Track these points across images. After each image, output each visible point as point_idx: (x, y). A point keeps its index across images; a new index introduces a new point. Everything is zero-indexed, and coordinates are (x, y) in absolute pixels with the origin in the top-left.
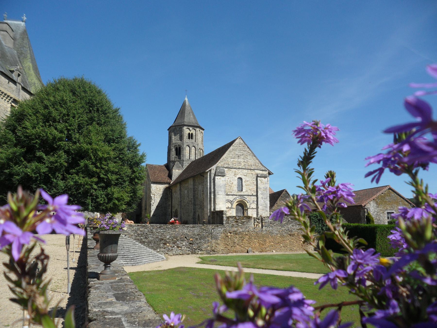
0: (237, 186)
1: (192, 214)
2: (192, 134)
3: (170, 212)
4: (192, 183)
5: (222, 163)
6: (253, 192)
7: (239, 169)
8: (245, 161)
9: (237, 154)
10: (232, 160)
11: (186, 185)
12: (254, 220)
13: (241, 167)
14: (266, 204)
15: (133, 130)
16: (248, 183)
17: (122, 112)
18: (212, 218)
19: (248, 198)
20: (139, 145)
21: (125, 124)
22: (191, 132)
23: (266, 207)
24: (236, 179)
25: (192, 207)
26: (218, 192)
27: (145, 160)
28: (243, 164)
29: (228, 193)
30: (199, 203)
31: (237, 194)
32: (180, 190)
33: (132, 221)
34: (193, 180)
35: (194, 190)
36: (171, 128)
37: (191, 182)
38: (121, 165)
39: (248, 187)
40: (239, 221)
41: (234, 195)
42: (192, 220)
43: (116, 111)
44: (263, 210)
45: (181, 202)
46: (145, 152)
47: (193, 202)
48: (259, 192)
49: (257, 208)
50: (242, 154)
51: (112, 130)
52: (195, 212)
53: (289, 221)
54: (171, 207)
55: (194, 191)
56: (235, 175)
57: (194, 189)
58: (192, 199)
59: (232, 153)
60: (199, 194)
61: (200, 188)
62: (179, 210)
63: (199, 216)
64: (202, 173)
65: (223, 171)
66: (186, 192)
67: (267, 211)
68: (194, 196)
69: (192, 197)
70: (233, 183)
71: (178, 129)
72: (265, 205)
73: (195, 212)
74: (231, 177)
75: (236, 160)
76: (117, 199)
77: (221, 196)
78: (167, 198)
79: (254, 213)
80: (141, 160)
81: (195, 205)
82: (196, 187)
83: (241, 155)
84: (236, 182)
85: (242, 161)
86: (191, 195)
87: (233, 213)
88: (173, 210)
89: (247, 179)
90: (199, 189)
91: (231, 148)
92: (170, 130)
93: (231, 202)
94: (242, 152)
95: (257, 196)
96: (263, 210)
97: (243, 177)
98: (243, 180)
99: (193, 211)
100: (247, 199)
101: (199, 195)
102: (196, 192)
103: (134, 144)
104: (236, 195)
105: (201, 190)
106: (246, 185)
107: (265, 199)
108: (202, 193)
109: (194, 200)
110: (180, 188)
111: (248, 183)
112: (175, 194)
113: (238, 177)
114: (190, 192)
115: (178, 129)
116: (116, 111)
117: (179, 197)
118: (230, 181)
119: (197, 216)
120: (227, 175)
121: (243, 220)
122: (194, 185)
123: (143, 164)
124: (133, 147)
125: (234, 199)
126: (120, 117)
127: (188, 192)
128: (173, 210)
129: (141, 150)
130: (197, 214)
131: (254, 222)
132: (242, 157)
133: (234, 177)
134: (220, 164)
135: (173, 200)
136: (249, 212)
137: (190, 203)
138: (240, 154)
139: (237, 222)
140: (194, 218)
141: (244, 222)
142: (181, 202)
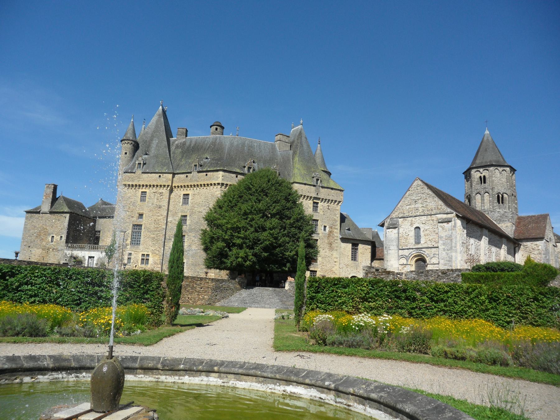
8: (424, 205)
10: (408, 207)
16: (428, 232)
24: (413, 229)
28: (421, 210)
31: (414, 247)
39: (427, 237)
53: (439, 276)
59: (408, 199)
72: (448, 259)
75: (413, 206)
83: (418, 199)
84: (412, 233)
85: (421, 205)
89: (426, 228)
111: (428, 232)
113: (415, 226)
132: (420, 201)
138: (417, 198)
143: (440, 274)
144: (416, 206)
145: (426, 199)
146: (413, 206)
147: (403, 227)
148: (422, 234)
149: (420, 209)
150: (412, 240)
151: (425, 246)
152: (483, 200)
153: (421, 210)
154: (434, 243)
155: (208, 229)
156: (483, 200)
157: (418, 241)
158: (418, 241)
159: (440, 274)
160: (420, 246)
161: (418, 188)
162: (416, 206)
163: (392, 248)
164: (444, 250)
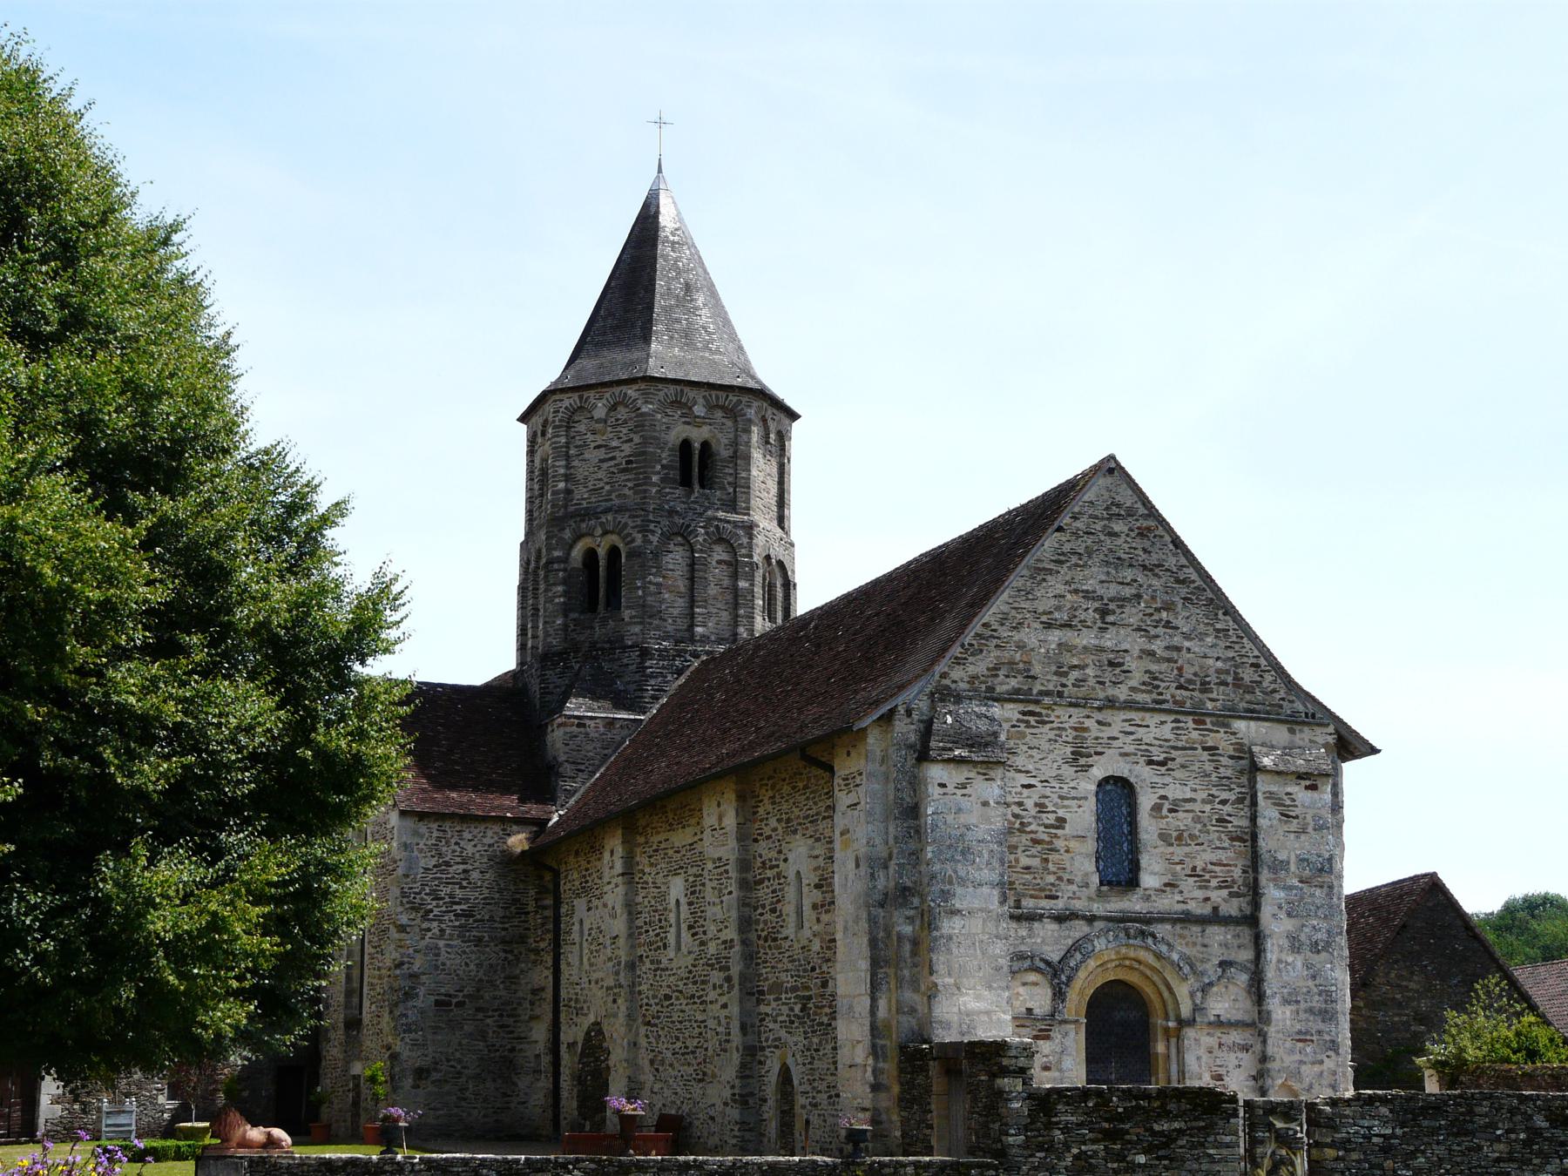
0: (1091, 846)
1: (728, 1068)
2: (705, 445)
3: (541, 1047)
4: (730, 821)
5: (979, 666)
6: (1218, 896)
7: (1111, 704)
8: (1157, 646)
9: (1088, 595)
10: (1055, 636)
11: (681, 838)
12: (1252, 1126)
13: (1122, 693)
14: (1328, 996)
15: (284, 403)
16: (1183, 820)
17: (199, 254)
18: (905, 1102)
19: (1181, 944)
20: (340, 508)
21: (223, 349)
22: (698, 435)
23: (1327, 1015)
24: (1088, 787)
25: (735, 1009)
26: (946, 895)
27: (392, 634)
28: (1137, 670)
29: (1028, 903)
30: (787, 980)
31: (1098, 908)
32: (628, 873)
33: (278, 1133)
34: (741, 798)
35: (750, 876)
36: (549, 408)
37: (719, 818)
38: (207, 672)
39: (1179, 852)
40: (1133, 1130)
41: (1073, 916)
42: (734, 1113)
43: (161, 238)
44: (1302, 1038)
45: (632, 966)
46: (391, 571)
47: (736, 970)
48: (1273, 894)
49: (1258, 1023)
50: (1128, 591)
51: (131, 387)
52: (752, 1054)
53: (1535, 1133)
54: (547, 1008)
55: (745, 885)
56: (1079, 757)
57: (744, 865)
58: (728, 944)
59: (1056, 585)
60: (789, 909)
61: (799, 856)
62: (617, 1032)
63: (785, 1076)
64: (817, 741)
65: (983, 726)
66: (677, 888)
67: (1334, 1046)
68: (745, 924)
69: (731, 934)
70: (1061, 822)
71: (600, 411)
72: (1317, 1002)
73: (752, 1054)
74: (1049, 771)
75: (1087, 638)
76: (178, 950)
77: (975, 925)
78: (522, 939)
79: (1231, 1059)
80: (367, 627)
81: (752, 992)
82: (764, 849)
83: (1122, 601)
84: (1083, 817)
85: (1135, 643)
86: (721, 911)
87: (1064, 1063)
88: (573, 1033)
89: (1175, 792)
90: (790, 870)
91: (1049, 544)
92: (537, 420)
93: (1057, 974)
94: (1128, 574)
95: (1251, 920)
96: (1302, 1038)
97: (1141, 774)
98: (1146, 801)
99: (736, 1038)
100: (1180, 946)
101: (791, 921)
102: (764, 893)
103: (293, 509)
104: (1091, 919)
105: (810, 878)
106: (1164, 837)
107: (1315, 948)
108: (811, 897)
109: (750, 957)
110: (629, 860)
111: (1183, 820)
112: (580, 904)
113: (1098, 773)
114: (710, 895)
115: (600, 411)
116: (161, 238)
117: (619, 926)
118: (1041, 807)
119: (773, 1078)
120: (1019, 761)
121: (1163, 1126)
122: (746, 837)
123: (375, 668)
124: (297, 530)
125: (1075, 947)
126: (188, 294)
127: (694, 891)
128: (567, 1035)
129: (355, 558)
130: (773, 1067)
131: (1253, 1142)
132: (1132, 615)
133: (1068, 771)
134: (957, 674)
135: (571, 955)
136: (1190, 1059)
137: (716, 977)
138: (1113, 590)
139: (1110, 1136)
140: (745, 1099)
141: (1169, 1139)
142: (632, 966)
143: (1540, 1122)
144: (1109, 640)
145: (1168, 607)
146: (1087, 638)
147: (1019, 761)
148: (1148, 828)
149: (1131, 663)
150: (1082, 862)
151: (1168, 903)
152: (693, 569)
153: (1137, 670)
154: (1218, 896)
155: (357, 667)
156: (693, 569)
157: (1120, 869)
158: (1120, 869)
159: (1540, 1122)
160: (1133, 904)
161: (1118, 526)
162: (1109, 640)
163: (964, 899)
164: (1295, 945)
